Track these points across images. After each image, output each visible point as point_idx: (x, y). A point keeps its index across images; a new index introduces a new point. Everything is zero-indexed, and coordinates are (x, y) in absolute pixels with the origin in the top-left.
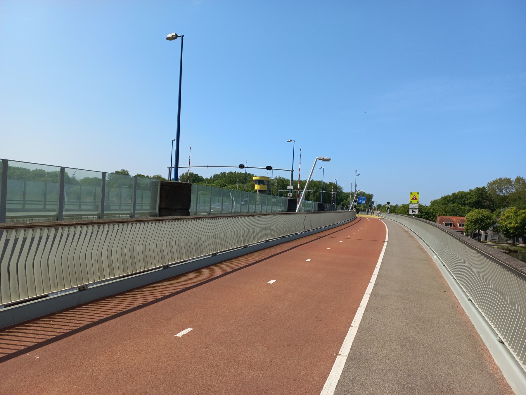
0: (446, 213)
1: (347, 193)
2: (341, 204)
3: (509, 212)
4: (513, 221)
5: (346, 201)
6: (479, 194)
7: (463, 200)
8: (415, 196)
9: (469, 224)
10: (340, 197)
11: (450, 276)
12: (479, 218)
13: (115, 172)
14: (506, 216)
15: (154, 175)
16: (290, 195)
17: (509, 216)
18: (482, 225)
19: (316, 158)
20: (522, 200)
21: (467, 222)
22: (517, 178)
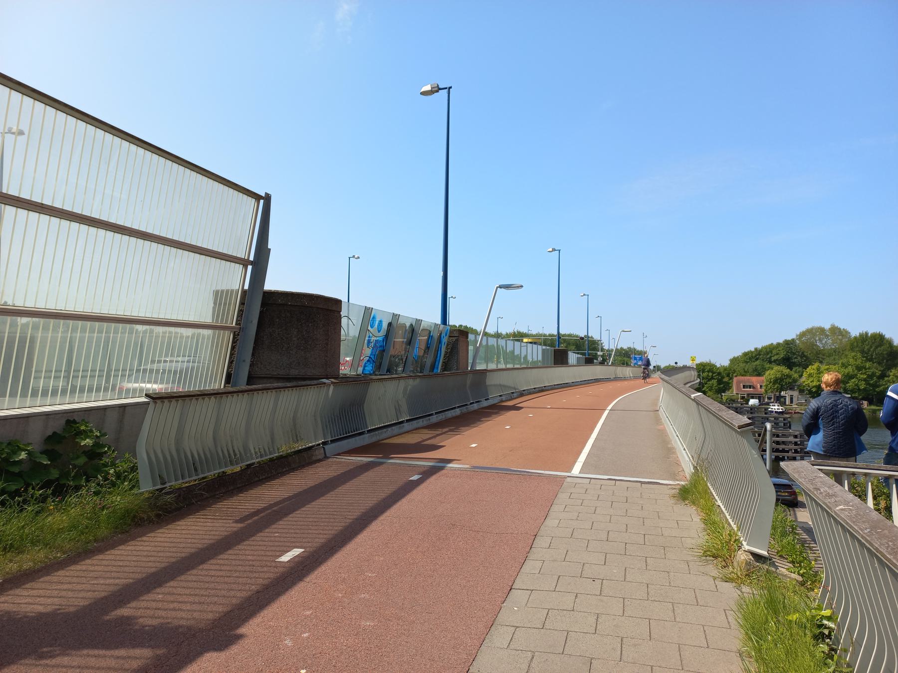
0: (745, 373)
7: (768, 356)
11: (669, 423)
13: (518, 332)
14: (808, 374)
22: (832, 328)
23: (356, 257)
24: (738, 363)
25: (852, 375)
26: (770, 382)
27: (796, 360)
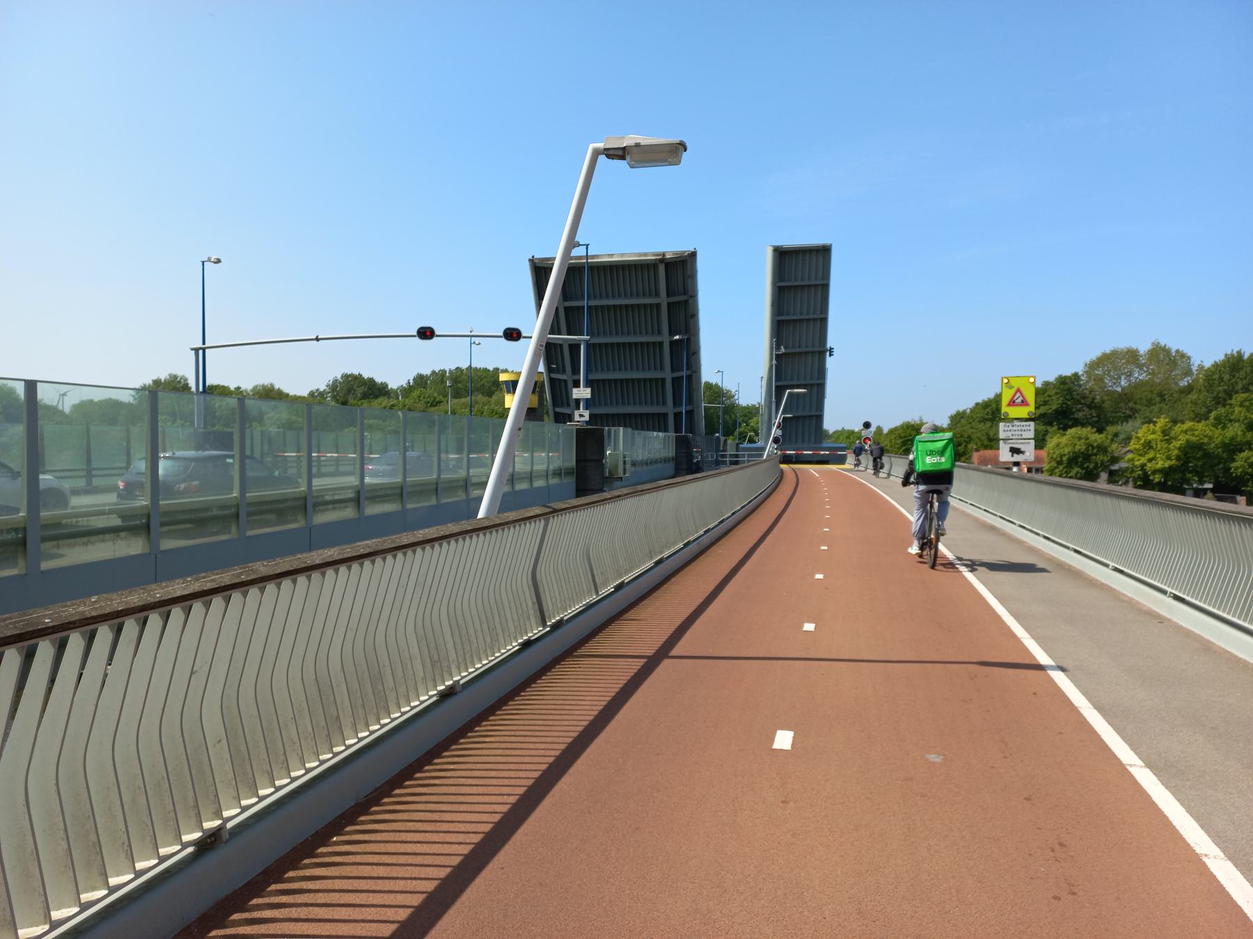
1: (747, 408)
2: (736, 433)
3: (1149, 430)
4: (1160, 454)
5: (747, 425)
6: (1065, 392)
8: (1018, 390)
9: (1055, 468)
10: (733, 416)
12: (1080, 450)
14: (1142, 442)
15: (255, 384)
16: (581, 416)
17: (1150, 442)
18: (1088, 467)
19: (592, 146)
20: (1167, 400)
21: (1049, 463)
23: (212, 260)
24: (970, 423)
25: (1241, 444)
26: (1060, 463)
27: (1081, 414)
